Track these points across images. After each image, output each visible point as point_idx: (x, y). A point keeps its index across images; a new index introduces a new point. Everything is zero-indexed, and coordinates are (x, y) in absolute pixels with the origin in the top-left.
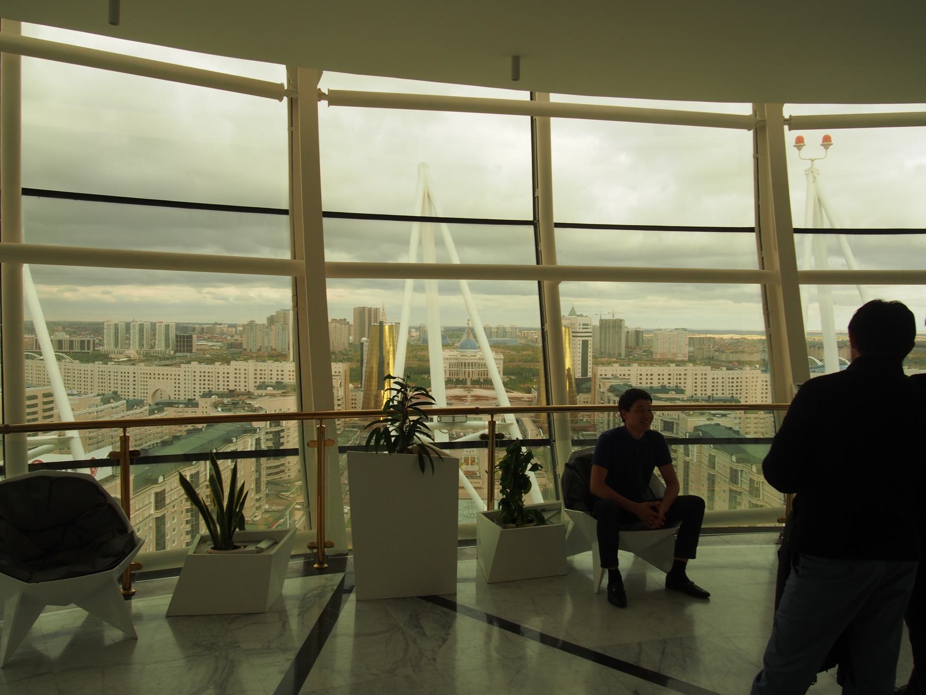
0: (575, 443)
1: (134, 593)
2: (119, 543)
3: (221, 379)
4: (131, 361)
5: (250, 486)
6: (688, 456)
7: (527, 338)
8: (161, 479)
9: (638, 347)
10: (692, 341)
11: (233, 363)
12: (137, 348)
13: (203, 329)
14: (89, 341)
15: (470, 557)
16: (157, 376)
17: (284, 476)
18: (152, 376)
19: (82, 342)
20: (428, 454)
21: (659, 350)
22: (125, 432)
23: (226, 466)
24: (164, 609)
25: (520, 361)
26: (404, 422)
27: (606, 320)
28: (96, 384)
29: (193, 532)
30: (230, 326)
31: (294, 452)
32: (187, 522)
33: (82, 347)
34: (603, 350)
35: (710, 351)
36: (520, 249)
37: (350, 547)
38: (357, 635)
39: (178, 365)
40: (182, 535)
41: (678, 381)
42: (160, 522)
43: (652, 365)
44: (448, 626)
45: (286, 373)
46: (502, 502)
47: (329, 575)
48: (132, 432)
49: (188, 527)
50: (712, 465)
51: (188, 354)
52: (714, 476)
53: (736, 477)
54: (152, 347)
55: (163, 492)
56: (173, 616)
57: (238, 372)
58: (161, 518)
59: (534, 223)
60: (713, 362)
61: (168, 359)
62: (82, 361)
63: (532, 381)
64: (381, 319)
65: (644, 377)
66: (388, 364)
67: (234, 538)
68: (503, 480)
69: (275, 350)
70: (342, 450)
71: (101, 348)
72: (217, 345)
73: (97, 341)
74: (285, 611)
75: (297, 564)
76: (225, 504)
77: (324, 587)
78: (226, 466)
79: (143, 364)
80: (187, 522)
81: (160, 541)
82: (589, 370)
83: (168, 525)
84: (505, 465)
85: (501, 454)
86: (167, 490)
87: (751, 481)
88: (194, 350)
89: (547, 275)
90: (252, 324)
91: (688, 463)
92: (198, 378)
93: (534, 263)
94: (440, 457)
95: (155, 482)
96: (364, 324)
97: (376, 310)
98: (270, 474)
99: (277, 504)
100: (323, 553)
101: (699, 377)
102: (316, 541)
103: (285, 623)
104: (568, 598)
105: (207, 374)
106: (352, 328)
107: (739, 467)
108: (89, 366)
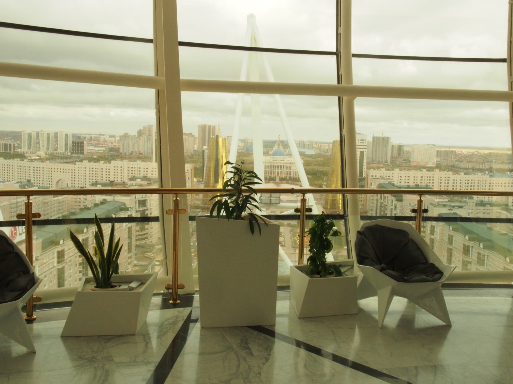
0: (363, 218)
1: (35, 319)
2: (23, 281)
3: (104, 173)
5: (124, 243)
7: (320, 149)
8: (61, 242)
9: (400, 158)
10: (439, 153)
12: (45, 150)
13: (91, 138)
17: (148, 241)
20: (257, 221)
21: (416, 159)
22: (28, 199)
23: (106, 228)
24: (60, 331)
25: (315, 165)
26: (238, 197)
27: (377, 138)
28: (16, 172)
30: (111, 136)
31: (156, 219)
32: (80, 272)
33: (6, 149)
34: (374, 158)
35: (452, 161)
36: (325, 70)
37: (197, 289)
38: (201, 354)
39: (74, 163)
40: (76, 281)
41: (428, 181)
42: (61, 273)
43: (409, 170)
44: (269, 349)
45: (150, 170)
46: (311, 259)
50: (450, 241)
51: (81, 156)
52: (451, 249)
53: (468, 251)
54: (56, 149)
56: (66, 337)
57: (116, 168)
58: (56, 267)
59: (337, 54)
60: (454, 169)
61: (67, 158)
62: (5, 158)
63: (322, 179)
64: (217, 133)
65: (403, 178)
67: (112, 280)
69: (142, 154)
70: (192, 218)
71: (19, 150)
73: (16, 145)
75: (157, 300)
77: (177, 317)
78: (106, 228)
79: (48, 162)
82: (364, 173)
83: (66, 274)
84: (313, 232)
85: (310, 224)
87: (479, 254)
88: (85, 152)
89: (345, 92)
90: (125, 136)
91: (433, 239)
92: (88, 172)
93: (335, 82)
95: (57, 243)
96: (205, 138)
97: (214, 127)
98: (139, 239)
99: (143, 255)
100: (176, 293)
101: (443, 179)
102: (171, 283)
104: (357, 331)
105: (94, 170)
106: (197, 140)
107: (471, 244)
108: (11, 162)
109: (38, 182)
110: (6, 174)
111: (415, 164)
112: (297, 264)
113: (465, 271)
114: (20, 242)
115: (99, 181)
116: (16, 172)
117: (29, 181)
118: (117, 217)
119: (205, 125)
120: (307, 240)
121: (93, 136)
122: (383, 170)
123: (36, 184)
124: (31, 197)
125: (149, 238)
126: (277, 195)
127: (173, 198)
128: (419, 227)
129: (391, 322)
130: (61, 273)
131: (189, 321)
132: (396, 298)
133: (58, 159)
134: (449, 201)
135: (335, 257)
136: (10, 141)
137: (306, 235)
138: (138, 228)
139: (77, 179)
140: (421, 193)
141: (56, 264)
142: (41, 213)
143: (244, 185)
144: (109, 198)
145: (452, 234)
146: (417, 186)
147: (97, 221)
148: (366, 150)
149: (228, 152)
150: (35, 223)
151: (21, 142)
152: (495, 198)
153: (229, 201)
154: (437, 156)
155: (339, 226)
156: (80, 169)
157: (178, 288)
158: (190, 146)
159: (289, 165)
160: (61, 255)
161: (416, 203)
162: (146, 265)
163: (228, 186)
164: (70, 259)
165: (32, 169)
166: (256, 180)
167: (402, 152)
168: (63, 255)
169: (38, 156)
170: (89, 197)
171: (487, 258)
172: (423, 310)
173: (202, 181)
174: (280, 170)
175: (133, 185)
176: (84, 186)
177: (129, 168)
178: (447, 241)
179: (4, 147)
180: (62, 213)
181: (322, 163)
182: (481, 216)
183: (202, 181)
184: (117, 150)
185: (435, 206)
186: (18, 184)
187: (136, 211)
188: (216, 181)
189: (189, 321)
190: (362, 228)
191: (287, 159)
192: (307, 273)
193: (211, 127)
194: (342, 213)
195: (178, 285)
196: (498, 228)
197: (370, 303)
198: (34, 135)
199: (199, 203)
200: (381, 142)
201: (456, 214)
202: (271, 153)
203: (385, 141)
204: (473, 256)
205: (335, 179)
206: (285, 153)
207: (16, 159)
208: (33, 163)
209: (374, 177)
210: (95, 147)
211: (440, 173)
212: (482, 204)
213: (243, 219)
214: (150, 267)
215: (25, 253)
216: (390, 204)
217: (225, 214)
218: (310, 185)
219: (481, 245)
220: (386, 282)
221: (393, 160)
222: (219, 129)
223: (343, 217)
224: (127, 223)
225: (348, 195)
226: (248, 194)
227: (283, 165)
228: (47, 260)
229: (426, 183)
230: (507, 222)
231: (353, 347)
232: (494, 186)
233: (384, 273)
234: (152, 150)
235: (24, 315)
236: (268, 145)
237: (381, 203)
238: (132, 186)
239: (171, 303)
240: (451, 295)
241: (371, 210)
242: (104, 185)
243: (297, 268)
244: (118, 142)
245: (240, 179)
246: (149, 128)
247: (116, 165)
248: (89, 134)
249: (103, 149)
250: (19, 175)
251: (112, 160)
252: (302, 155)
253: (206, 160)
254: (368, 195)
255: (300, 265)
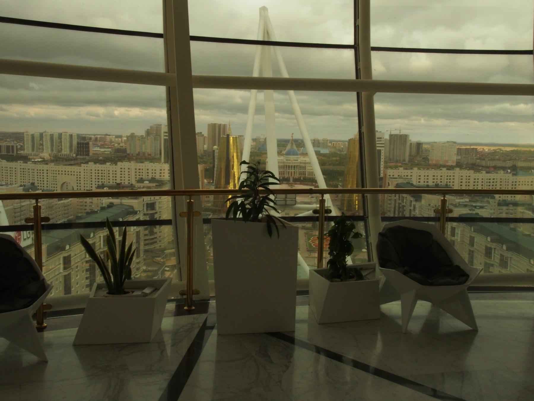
0: (384, 219)
1: (45, 327)
3: (111, 175)
4: (45, 162)
6: (454, 236)
8: (67, 247)
9: (419, 156)
11: (119, 164)
12: (50, 152)
13: (96, 138)
14: (13, 147)
15: (303, 304)
16: (64, 173)
17: (157, 246)
18: (60, 172)
19: (8, 147)
20: (274, 222)
21: (435, 157)
22: (323, 197)
24: (72, 339)
25: (330, 165)
27: (396, 135)
29: (92, 279)
30: (117, 137)
31: (167, 222)
32: (87, 278)
33: (8, 151)
35: (473, 159)
37: (212, 294)
39: (79, 164)
40: (83, 288)
41: (448, 181)
42: (67, 280)
43: (428, 169)
44: (289, 356)
46: (330, 262)
47: (196, 315)
48: (42, 203)
49: (88, 282)
50: (472, 242)
51: (87, 157)
52: (473, 252)
53: (490, 253)
54: (60, 151)
55: (69, 257)
56: (78, 345)
57: (123, 170)
58: (66, 271)
60: (474, 167)
61: (72, 160)
62: (8, 160)
65: (422, 177)
66: (233, 166)
67: (125, 285)
68: (331, 245)
69: (150, 155)
70: (207, 221)
71: (22, 152)
72: (108, 151)
73: (19, 147)
74: (164, 342)
75: (171, 306)
76: (118, 256)
79: (53, 164)
80: (87, 278)
81: (67, 288)
82: (382, 172)
83: (73, 281)
84: (333, 233)
86: (72, 255)
88: (91, 154)
89: (364, 87)
90: (132, 137)
92: (93, 174)
94: (284, 226)
95: (63, 249)
96: (215, 135)
97: (225, 126)
99: (157, 260)
100: (191, 299)
101: (464, 178)
102: (186, 289)
103: (163, 351)
104: (379, 337)
105: (100, 172)
106: (206, 139)
107: (493, 245)
108: (13, 165)
109: (42, 185)
110: (9, 177)
111: (434, 162)
112: (316, 268)
113: (487, 274)
114: (29, 247)
115: (105, 183)
116: (19, 175)
117: (33, 184)
118: (125, 220)
119: (215, 124)
120: (326, 243)
121: (99, 136)
122: (401, 169)
123: (40, 188)
124: (325, 195)
125: (158, 242)
126: (293, 196)
127: (186, 200)
128: (443, 228)
129: (415, 327)
130: (67, 280)
131: (205, 328)
132: (419, 303)
133: (62, 161)
134: (470, 201)
135: (353, 260)
136: (12, 143)
137: (325, 237)
138: (147, 232)
139: (82, 182)
140: (444, 192)
141: (61, 271)
142: (50, 217)
143: (260, 186)
144: (116, 201)
145: (473, 236)
146: (437, 185)
147: (108, 224)
148: (383, 148)
149: (240, 153)
150: (44, 227)
151: (24, 143)
152: (519, 198)
153: (246, 202)
154: (458, 154)
155: (360, 227)
156: (86, 171)
157: (193, 294)
158: (202, 146)
159: (304, 165)
160: (67, 261)
161: (440, 204)
162: (156, 270)
163: (244, 187)
164: (76, 265)
165: (36, 171)
166: (271, 180)
167: (421, 150)
168: (70, 262)
169: (41, 158)
170: (95, 200)
171: (510, 261)
172: (448, 314)
173: (213, 182)
174: (293, 171)
175: (146, 186)
176: (91, 189)
177: (136, 169)
178: (468, 242)
179: (4, 148)
180: (67, 217)
181: (337, 163)
182: (504, 216)
183: (213, 182)
184: (124, 151)
185: (455, 206)
186: (22, 188)
187: (145, 214)
188: (227, 183)
189: (205, 328)
190: (384, 229)
191: (301, 159)
192: (327, 277)
193: (222, 126)
194: (361, 214)
195: (192, 291)
196: (522, 229)
197: (393, 308)
198: (37, 136)
199: (209, 205)
200: (399, 140)
201: (477, 214)
202: (284, 152)
203: (403, 138)
204: (496, 259)
205: (351, 180)
206: (299, 153)
207: (19, 162)
208: (37, 165)
209: (391, 176)
210: (101, 148)
211: (461, 171)
212: (505, 203)
213: (260, 221)
214: (160, 272)
215: (34, 258)
216: (409, 204)
217: (241, 216)
218: (327, 187)
219: (504, 247)
220: (411, 285)
221: (412, 158)
222: (229, 128)
223: (363, 218)
224: (135, 227)
225: (368, 195)
226: (264, 195)
227: (296, 165)
228: (53, 266)
229: (445, 183)
230: (489, 222)
231: (376, 353)
232: (517, 185)
233: (408, 277)
234: (160, 151)
235: (35, 323)
236: (282, 144)
237: (399, 204)
238: (140, 188)
239: (186, 310)
240: (477, 299)
241: (389, 211)
242: (110, 187)
243: (316, 271)
244: (125, 142)
245: (257, 179)
246: (157, 128)
247: (123, 167)
248: (95, 135)
249: (110, 150)
250: (22, 178)
251: (118, 161)
252: (318, 153)
253: (216, 160)
254: (386, 195)
255: (319, 269)
